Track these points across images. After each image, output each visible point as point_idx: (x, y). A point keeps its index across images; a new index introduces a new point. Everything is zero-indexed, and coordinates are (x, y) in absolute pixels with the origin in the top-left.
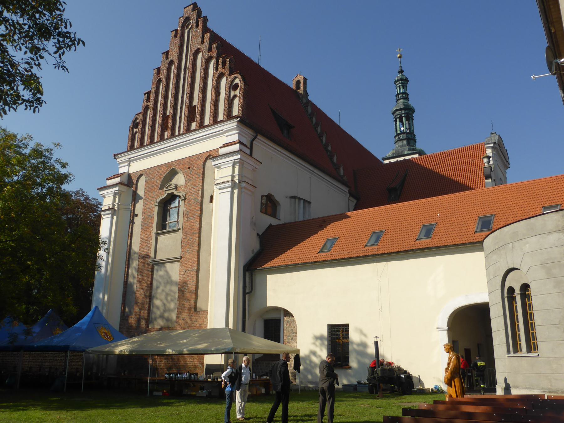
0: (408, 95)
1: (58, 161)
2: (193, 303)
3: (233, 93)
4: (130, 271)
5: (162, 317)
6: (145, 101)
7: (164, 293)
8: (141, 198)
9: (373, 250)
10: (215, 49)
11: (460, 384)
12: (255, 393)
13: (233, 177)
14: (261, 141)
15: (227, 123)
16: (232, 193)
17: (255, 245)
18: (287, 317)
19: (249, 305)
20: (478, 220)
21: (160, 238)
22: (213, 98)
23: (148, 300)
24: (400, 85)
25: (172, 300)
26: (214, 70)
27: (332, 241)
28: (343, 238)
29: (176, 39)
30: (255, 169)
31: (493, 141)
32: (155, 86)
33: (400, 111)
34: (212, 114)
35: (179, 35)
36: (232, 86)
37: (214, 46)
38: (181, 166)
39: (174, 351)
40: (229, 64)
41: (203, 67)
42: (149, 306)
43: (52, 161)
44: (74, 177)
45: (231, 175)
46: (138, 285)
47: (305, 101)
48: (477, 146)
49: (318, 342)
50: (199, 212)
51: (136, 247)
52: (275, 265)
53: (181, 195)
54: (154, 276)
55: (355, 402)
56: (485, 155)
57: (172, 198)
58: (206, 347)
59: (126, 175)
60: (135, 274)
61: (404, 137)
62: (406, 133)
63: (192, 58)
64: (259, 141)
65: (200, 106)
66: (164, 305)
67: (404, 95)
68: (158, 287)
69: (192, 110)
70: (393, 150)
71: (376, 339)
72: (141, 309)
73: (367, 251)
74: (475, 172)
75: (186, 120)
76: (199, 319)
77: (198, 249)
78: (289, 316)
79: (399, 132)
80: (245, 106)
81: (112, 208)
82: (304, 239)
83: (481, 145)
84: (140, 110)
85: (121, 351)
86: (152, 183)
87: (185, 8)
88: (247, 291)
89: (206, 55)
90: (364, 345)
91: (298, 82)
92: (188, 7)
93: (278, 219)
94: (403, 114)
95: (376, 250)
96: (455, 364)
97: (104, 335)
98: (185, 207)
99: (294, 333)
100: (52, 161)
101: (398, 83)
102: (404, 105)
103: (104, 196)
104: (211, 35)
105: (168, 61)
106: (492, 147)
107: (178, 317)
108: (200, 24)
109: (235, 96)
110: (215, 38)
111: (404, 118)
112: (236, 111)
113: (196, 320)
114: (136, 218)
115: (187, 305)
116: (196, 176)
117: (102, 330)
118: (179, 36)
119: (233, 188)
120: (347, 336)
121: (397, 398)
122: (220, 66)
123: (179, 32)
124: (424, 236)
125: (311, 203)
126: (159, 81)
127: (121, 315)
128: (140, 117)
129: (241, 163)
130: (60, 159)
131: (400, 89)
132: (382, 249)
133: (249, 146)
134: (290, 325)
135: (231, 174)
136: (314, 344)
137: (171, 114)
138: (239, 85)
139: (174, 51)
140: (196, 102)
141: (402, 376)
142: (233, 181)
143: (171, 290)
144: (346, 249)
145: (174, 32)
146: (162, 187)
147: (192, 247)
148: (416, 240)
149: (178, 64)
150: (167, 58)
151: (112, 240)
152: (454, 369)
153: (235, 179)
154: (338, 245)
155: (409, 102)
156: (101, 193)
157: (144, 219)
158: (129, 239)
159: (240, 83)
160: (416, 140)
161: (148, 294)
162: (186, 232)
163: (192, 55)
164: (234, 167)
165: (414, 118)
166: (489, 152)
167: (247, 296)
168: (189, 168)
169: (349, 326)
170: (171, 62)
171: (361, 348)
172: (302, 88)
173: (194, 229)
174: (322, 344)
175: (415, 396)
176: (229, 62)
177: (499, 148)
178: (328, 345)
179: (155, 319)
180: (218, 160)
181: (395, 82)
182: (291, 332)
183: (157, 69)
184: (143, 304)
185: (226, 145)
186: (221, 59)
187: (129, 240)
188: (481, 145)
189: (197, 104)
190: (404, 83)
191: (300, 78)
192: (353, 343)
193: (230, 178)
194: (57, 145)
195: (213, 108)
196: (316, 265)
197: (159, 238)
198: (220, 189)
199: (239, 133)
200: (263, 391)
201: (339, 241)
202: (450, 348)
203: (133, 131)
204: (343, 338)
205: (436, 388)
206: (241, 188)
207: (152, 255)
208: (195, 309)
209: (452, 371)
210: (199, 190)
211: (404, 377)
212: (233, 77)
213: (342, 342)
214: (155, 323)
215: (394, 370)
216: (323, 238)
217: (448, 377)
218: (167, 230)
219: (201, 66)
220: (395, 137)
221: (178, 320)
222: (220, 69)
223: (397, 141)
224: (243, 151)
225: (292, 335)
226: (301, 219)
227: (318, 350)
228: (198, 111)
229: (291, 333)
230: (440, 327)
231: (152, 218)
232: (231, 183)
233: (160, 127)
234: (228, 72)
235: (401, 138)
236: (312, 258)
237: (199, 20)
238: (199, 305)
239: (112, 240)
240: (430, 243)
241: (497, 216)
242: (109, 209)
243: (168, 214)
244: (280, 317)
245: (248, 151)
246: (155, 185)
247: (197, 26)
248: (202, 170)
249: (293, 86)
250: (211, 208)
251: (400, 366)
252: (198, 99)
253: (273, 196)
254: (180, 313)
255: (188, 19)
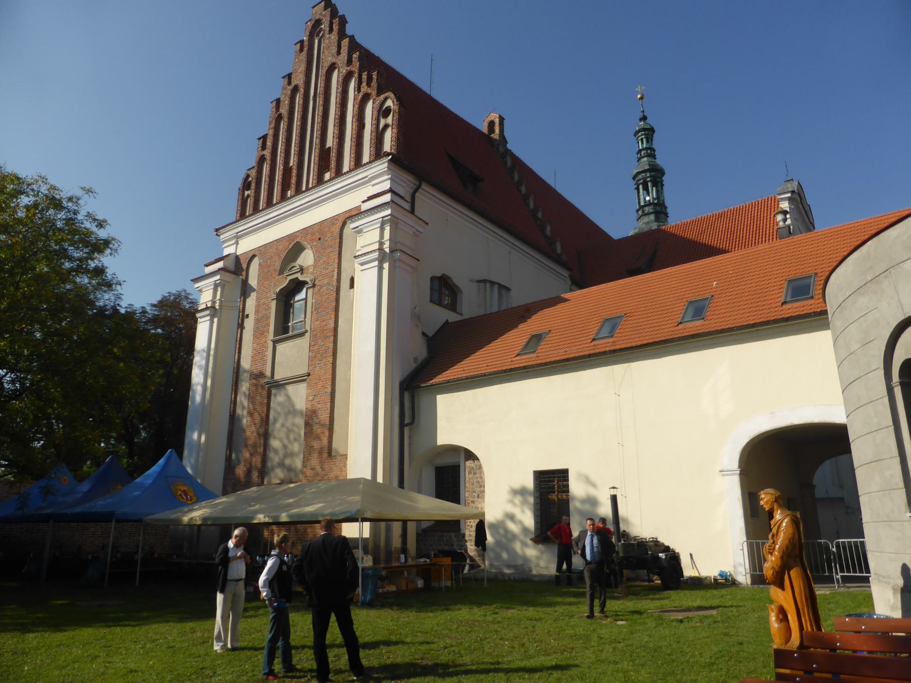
0: (654, 151)
1: (89, 215)
2: (325, 441)
3: (382, 122)
4: (238, 399)
5: (281, 465)
6: (260, 149)
7: (285, 430)
8: (254, 290)
9: (605, 345)
10: (357, 60)
11: (803, 581)
12: (404, 587)
13: (381, 244)
14: (429, 193)
15: (374, 164)
16: (381, 269)
17: (421, 351)
18: (469, 462)
19: (410, 444)
20: (785, 285)
21: (281, 347)
22: (354, 132)
23: (262, 442)
24: (643, 137)
25: (295, 439)
26: (355, 92)
27: (537, 339)
28: (556, 331)
29: (302, 54)
30: (417, 233)
31: (790, 189)
32: (273, 125)
33: (644, 174)
34: (353, 156)
35: (306, 48)
36: (381, 112)
37: (355, 56)
38: (309, 237)
39: (268, 517)
40: (377, 79)
41: (340, 89)
42: (265, 450)
43: (80, 217)
44: (120, 244)
45: (379, 241)
46: (249, 419)
47: (501, 150)
48: (763, 201)
49: (518, 499)
50: (334, 304)
51: (246, 363)
52: (448, 378)
53: (308, 280)
54: (272, 404)
55: (574, 608)
56: (780, 210)
57: (297, 286)
58: (317, 510)
59: (232, 258)
60: (246, 403)
61: (651, 211)
62: (653, 204)
63: (323, 78)
64: (427, 194)
65: (335, 147)
66: (285, 447)
67: (649, 151)
68: (275, 421)
69: (324, 154)
70: (635, 228)
71: (613, 492)
72: (251, 455)
73: (595, 348)
74: (762, 238)
75: (316, 170)
76: (334, 468)
77: (333, 361)
78: (474, 460)
79: (642, 204)
80: (402, 139)
81: (211, 307)
82: (495, 338)
83: (770, 199)
84: (253, 163)
85: (191, 519)
86: (268, 267)
87: (313, 7)
88: (407, 421)
89: (344, 71)
90: (593, 502)
91: (492, 124)
92: (318, 6)
93: (458, 313)
94: (648, 177)
95: (610, 344)
96: (790, 536)
97: (180, 495)
98: (314, 297)
99: (481, 486)
100: (80, 217)
101: (640, 134)
102: (649, 165)
103: (201, 291)
104: (350, 42)
105: (290, 87)
106: (789, 199)
107: (304, 466)
108: (335, 27)
109: (386, 126)
110: (354, 46)
111: (650, 184)
112: (387, 146)
113: (331, 470)
114: (246, 320)
115: (316, 444)
116: (329, 250)
117: (179, 487)
118: (306, 49)
119: (381, 261)
120: (565, 489)
121: (654, 596)
122: (364, 84)
123: (306, 43)
124: (693, 317)
125: (510, 290)
126: (279, 118)
127: (225, 465)
128: (253, 173)
129: (394, 221)
130: (94, 214)
131: (642, 143)
132: (620, 343)
133: (408, 198)
134: (475, 474)
135: (378, 239)
136: (511, 502)
137: (295, 163)
138: (392, 107)
139: (300, 71)
140: (330, 142)
141: (662, 555)
142: (381, 249)
143: (294, 424)
144: (560, 347)
145: (299, 45)
146: (281, 272)
147: (325, 357)
148: (678, 324)
149: (305, 89)
150: (289, 83)
151: (212, 353)
152: (787, 547)
153: (385, 246)
154: (548, 342)
155: (656, 161)
156: (197, 285)
157: (257, 321)
158: (237, 352)
159: (394, 105)
160: (668, 213)
161: (262, 431)
162: (315, 336)
163: (324, 73)
164: (382, 229)
165: (664, 183)
166: (785, 205)
167: (406, 430)
168: (320, 239)
169: (568, 473)
170: (295, 89)
171: (587, 507)
172: (497, 130)
173: (326, 330)
174: (524, 502)
175: (687, 592)
176: (377, 77)
177: (799, 200)
178: (535, 504)
179: (273, 468)
180: (359, 219)
181: (635, 133)
182: (476, 485)
183: (275, 102)
184: (255, 446)
185: (370, 198)
186: (366, 73)
187: (237, 354)
188: (770, 199)
189: (331, 146)
190: (648, 134)
191: (495, 117)
192: (574, 498)
193: (376, 246)
194: (89, 191)
195: (354, 148)
196: (512, 374)
197: (277, 347)
198: (362, 264)
199: (391, 179)
200: (420, 583)
201: (549, 335)
202: (776, 501)
203: (243, 194)
204: (559, 492)
205: (722, 576)
206: (395, 261)
207: (268, 373)
208: (328, 453)
209: (784, 552)
210: (334, 271)
211: (666, 558)
212: (382, 97)
213: (558, 498)
214: (272, 475)
215: (646, 546)
216: (526, 334)
217: (775, 565)
218: (291, 333)
219: (337, 88)
220: (637, 211)
221: (305, 470)
222: (364, 88)
223: (640, 217)
224: (395, 203)
225: (478, 489)
226: (495, 309)
227: (517, 511)
228: (333, 155)
229: (477, 487)
230: (726, 468)
231: (268, 318)
232: (378, 253)
233: (280, 184)
234: (376, 91)
235: (646, 212)
236: (507, 364)
237: (334, 21)
238: (334, 445)
239: (212, 353)
240: (703, 327)
241: (819, 275)
242: (207, 308)
243: (292, 311)
244: (459, 462)
245: (407, 206)
246: (272, 268)
247: (331, 30)
248: (338, 240)
249: (484, 129)
250: (352, 297)
251: (657, 539)
252: (333, 137)
253: (449, 278)
254: (308, 459)
255: (318, 22)
